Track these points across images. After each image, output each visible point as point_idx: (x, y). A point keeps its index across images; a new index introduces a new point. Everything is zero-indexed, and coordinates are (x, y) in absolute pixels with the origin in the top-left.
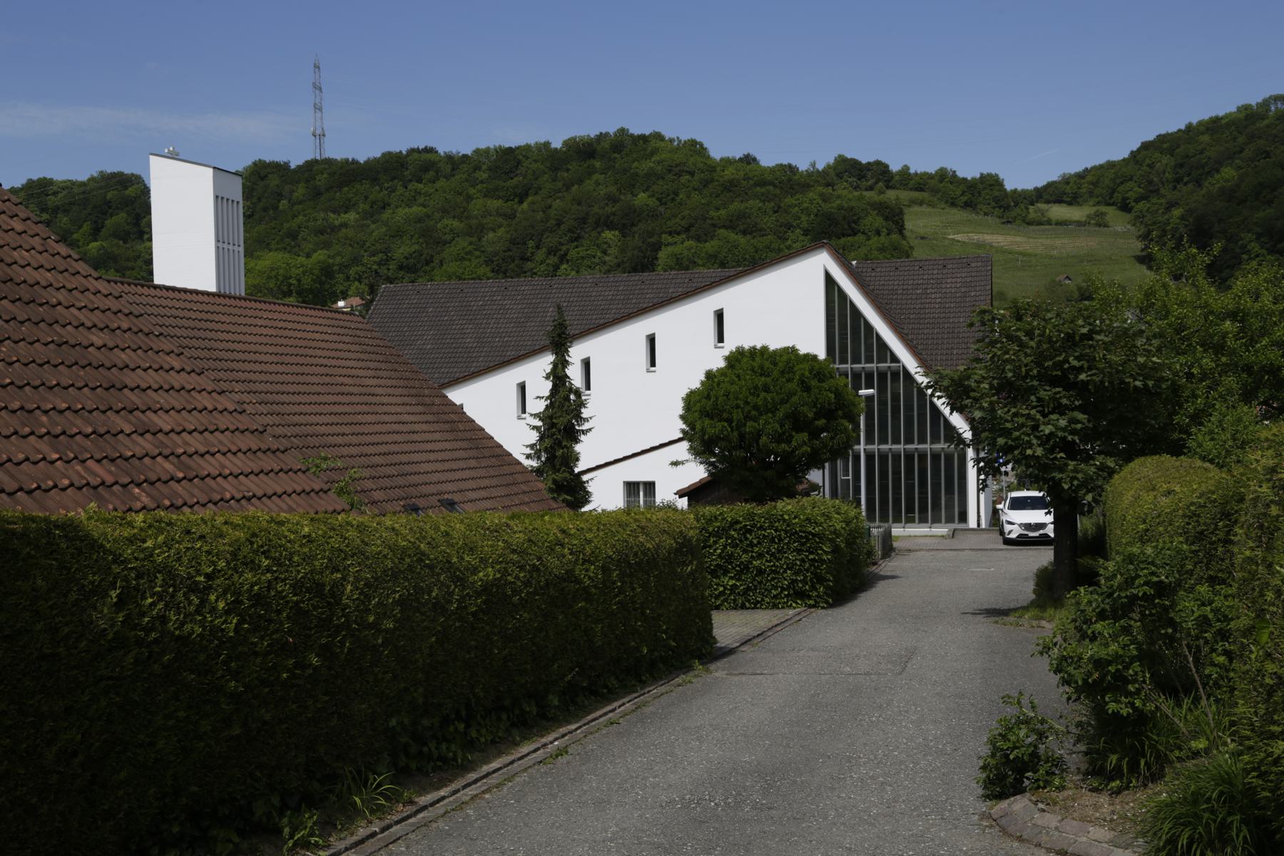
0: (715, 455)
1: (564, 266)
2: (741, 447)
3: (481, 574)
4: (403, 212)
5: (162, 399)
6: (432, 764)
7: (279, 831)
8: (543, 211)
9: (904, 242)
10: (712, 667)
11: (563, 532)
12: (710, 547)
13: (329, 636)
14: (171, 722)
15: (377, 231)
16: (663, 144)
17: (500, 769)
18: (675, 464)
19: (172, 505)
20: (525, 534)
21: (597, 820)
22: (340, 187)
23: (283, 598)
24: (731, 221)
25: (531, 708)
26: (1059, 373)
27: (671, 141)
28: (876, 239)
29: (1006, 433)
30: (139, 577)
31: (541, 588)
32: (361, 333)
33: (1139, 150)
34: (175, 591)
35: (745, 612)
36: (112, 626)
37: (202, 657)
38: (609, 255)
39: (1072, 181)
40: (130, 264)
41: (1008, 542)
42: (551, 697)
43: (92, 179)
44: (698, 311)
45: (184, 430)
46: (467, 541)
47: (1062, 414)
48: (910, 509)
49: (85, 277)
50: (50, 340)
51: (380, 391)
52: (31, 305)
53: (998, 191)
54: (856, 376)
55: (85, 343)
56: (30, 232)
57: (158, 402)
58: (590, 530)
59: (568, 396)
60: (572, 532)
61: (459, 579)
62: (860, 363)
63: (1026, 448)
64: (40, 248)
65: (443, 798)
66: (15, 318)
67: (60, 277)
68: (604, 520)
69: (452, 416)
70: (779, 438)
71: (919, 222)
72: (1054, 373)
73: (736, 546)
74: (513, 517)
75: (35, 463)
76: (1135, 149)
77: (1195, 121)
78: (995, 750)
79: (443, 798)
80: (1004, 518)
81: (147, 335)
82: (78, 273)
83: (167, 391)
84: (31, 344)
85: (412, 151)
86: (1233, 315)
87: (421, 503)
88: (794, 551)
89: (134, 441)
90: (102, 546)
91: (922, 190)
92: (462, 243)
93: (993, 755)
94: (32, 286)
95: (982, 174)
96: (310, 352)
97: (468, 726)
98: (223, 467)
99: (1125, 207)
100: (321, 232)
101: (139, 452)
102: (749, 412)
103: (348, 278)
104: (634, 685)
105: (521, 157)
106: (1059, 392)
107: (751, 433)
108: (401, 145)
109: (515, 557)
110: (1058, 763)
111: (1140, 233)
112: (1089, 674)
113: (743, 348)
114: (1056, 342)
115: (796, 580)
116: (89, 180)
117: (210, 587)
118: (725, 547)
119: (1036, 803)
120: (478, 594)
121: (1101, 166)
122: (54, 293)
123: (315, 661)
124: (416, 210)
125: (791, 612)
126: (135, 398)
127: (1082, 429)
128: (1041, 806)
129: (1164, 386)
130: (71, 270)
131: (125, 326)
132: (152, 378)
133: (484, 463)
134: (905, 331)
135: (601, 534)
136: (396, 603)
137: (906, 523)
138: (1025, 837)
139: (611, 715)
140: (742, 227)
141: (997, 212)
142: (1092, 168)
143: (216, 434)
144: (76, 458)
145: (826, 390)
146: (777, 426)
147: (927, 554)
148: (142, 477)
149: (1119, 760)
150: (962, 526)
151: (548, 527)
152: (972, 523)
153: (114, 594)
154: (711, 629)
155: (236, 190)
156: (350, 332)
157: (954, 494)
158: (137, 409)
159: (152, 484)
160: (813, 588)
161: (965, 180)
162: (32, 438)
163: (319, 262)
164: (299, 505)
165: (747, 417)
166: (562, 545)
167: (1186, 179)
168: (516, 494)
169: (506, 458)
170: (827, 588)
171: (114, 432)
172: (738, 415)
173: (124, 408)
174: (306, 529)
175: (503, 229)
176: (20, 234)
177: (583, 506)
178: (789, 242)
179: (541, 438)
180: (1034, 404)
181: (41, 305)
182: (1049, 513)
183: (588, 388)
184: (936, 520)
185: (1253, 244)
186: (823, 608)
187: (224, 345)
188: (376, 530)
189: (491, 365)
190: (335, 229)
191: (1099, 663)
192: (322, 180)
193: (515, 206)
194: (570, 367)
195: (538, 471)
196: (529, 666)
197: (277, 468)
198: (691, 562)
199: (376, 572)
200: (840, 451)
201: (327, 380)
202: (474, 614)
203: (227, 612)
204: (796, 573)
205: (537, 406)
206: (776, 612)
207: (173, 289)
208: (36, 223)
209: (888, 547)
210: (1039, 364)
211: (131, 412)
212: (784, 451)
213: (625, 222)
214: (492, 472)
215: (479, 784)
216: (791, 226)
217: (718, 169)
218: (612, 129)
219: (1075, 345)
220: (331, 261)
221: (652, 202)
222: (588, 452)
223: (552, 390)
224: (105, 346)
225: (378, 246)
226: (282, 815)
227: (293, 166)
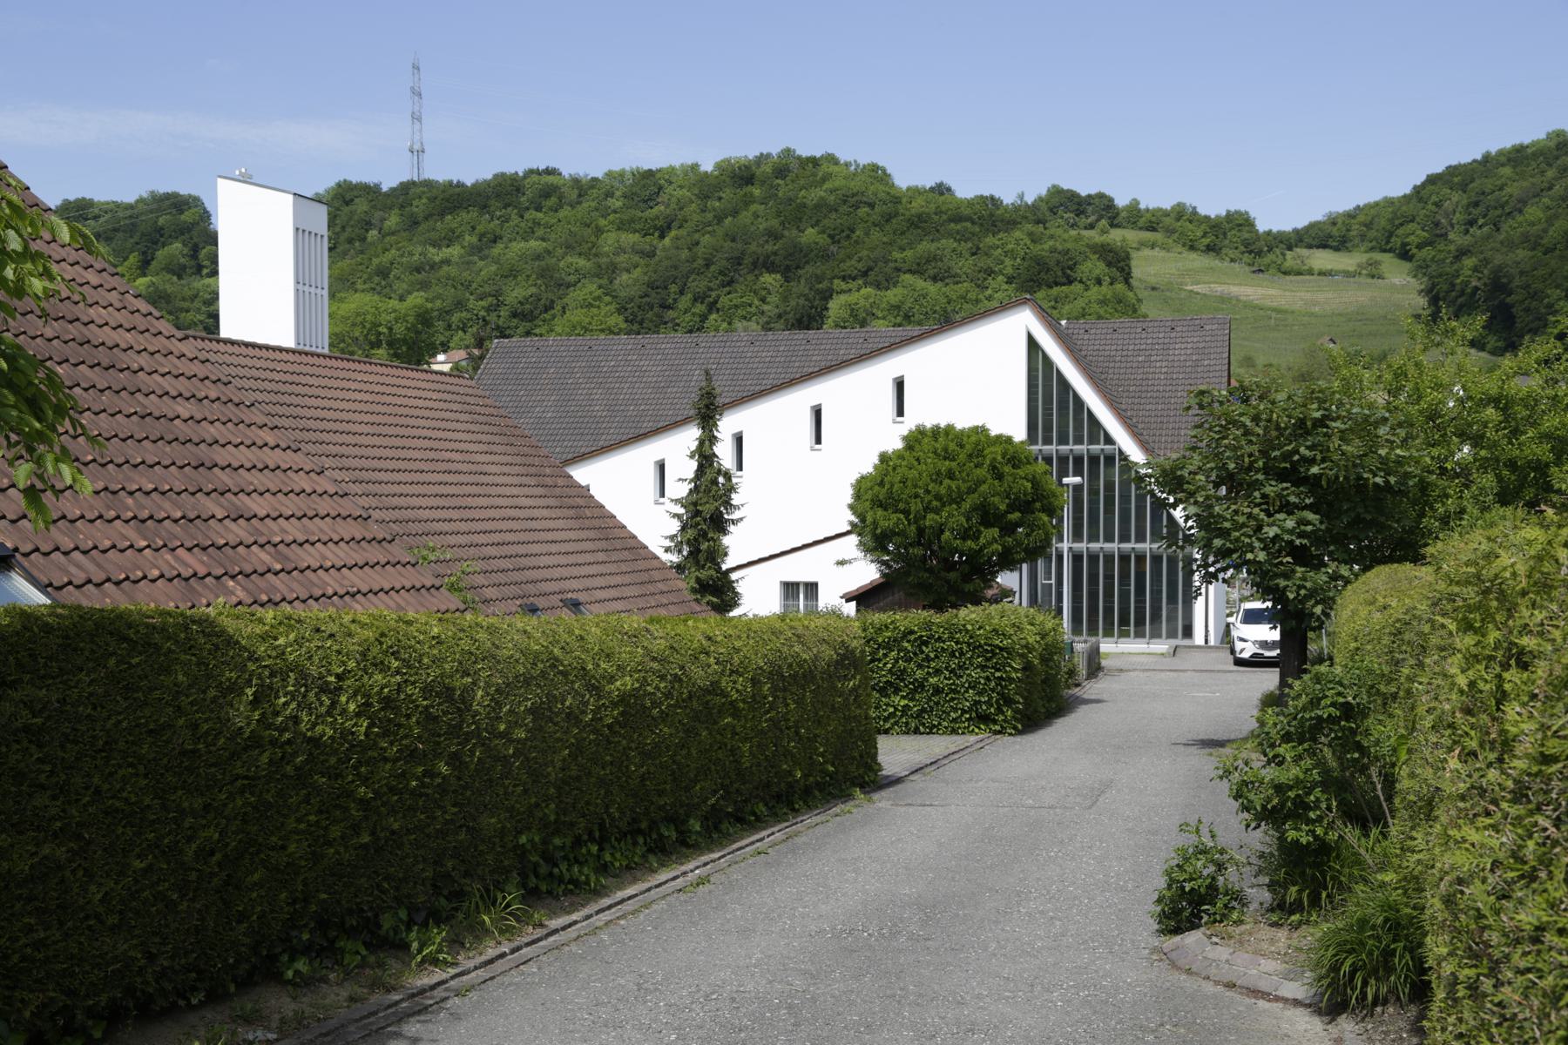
0: (888, 553)
1: (713, 316)
2: (919, 543)
3: (618, 683)
4: (518, 246)
5: (257, 480)
6: (563, 887)
7: (406, 947)
8: (690, 249)
9: (1131, 294)
10: (876, 796)
11: (709, 639)
12: (879, 660)
13: (459, 744)
14: (302, 826)
15: (488, 269)
16: (836, 168)
17: (636, 895)
18: (841, 563)
19: (270, 601)
20: (666, 640)
21: (741, 947)
22: (442, 215)
23: (413, 702)
24: (918, 264)
25: (670, 833)
26: (1288, 465)
27: (847, 165)
28: (1096, 289)
29: (1224, 534)
30: (272, 675)
31: (683, 701)
32: (472, 400)
33: (1424, 185)
34: (307, 691)
35: (919, 737)
36: (248, 724)
37: (333, 760)
38: (768, 303)
39: (1340, 221)
40: (186, 305)
41: (1240, 662)
42: (692, 821)
43: (141, 200)
44: (874, 378)
45: (281, 516)
46: (604, 647)
47: (1290, 513)
48: (1124, 621)
49: (168, 338)
50: (133, 411)
51: (493, 469)
52: (111, 370)
53: (1249, 232)
54: (1063, 460)
55: (170, 415)
56: (107, 286)
57: (251, 483)
58: (739, 637)
59: (716, 479)
60: (719, 638)
61: (595, 688)
62: (1067, 444)
63: (1246, 552)
64: (118, 305)
65: (575, 922)
66: (94, 386)
67: (140, 338)
68: (757, 628)
69: (578, 500)
70: (965, 535)
71: (1150, 266)
72: (1283, 465)
73: (909, 660)
74: (651, 621)
75: (122, 551)
76: (1419, 183)
77: (1493, 150)
78: (1171, 882)
79: (575, 922)
80: (1235, 633)
81: (237, 405)
82: (160, 333)
83: (261, 470)
84: (112, 415)
85: (531, 172)
86: (1495, 401)
87: (541, 603)
88: (978, 667)
89: (226, 528)
90: (237, 642)
91: (1154, 230)
92: (590, 288)
93: (1169, 887)
94: (111, 349)
95: (1228, 212)
96: (412, 422)
97: (601, 849)
98: (325, 558)
99: (1405, 255)
100: (418, 270)
101: (233, 541)
102: (930, 502)
103: (449, 327)
104: (785, 814)
105: (662, 182)
106: (1287, 488)
107: (931, 527)
108: (516, 164)
109: (655, 665)
110: (1238, 897)
111: (1423, 287)
112: (1269, 800)
113: (924, 427)
114: (1285, 429)
115: (980, 701)
116: (137, 201)
117: (341, 688)
118: (896, 661)
119: (1210, 937)
120: (615, 705)
121: (1377, 204)
122: (135, 356)
123: (444, 769)
124: (534, 244)
125: (972, 738)
126: (225, 478)
127: (1312, 531)
128: (1215, 939)
129: (1411, 483)
130: (153, 331)
131: (213, 395)
132: (244, 456)
133: (615, 556)
134: (1123, 407)
135: (751, 642)
136: (529, 711)
137: (1152, 637)
138: (1194, 970)
139: (758, 844)
140: (931, 272)
141: (1246, 258)
142: (1365, 205)
143: (316, 520)
144: (165, 546)
145: (1021, 478)
146: (963, 520)
147: (1141, 674)
148: (237, 569)
149: (1300, 892)
150: (1186, 642)
151: (692, 632)
152: (1199, 639)
153: (249, 691)
154: (876, 754)
155: (319, 219)
156: (458, 398)
157: (1177, 603)
158: (229, 490)
159: (247, 576)
160: (1000, 711)
161: (1207, 218)
162: (117, 522)
163: (415, 306)
164: (408, 603)
165: (927, 509)
166: (707, 654)
167: (1481, 221)
168: (653, 594)
169: (641, 551)
170: (1016, 711)
171: (204, 516)
172: (916, 506)
173: (215, 490)
174: (436, 630)
175: (639, 269)
176: (95, 288)
177: (729, 611)
178: (989, 292)
179: (683, 529)
180: (1258, 501)
181: (121, 371)
182: (1275, 628)
183: (740, 468)
184: (1156, 635)
185: (1561, 303)
186: (1010, 734)
187: (312, 413)
188: (507, 632)
189: (624, 438)
190: (434, 266)
191: (1279, 788)
192: (419, 207)
193: (655, 242)
194: (719, 444)
195: (679, 568)
196: (668, 787)
197: (383, 561)
198: (854, 677)
199: (507, 678)
200: (1037, 551)
201: (432, 455)
202: (610, 727)
203: (358, 715)
204: (980, 694)
205: (679, 489)
206: (955, 737)
207: (254, 346)
208: (113, 275)
209: (1095, 667)
210: (1264, 453)
211: (222, 494)
212: (970, 549)
213: (789, 265)
214: (624, 567)
215: (613, 910)
216: (993, 272)
217: (904, 200)
218: (775, 149)
219: (1308, 433)
220: (429, 305)
221: (823, 240)
222: (738, 545)
223: (697, 471)
224: (192, 418)
225: (487, 289)
226: (409, 929)
227: (385, 188)
